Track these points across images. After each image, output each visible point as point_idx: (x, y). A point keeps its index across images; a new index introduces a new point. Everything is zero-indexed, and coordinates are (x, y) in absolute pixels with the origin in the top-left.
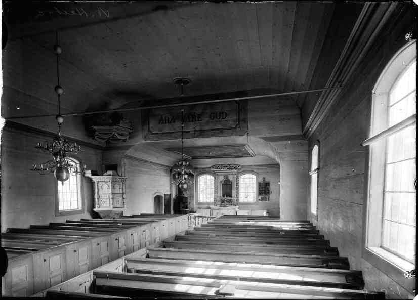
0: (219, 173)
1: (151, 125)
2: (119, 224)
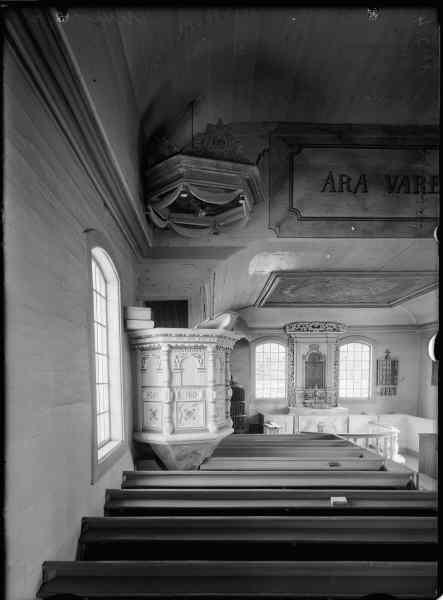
0: (302, 340)
1: (297, 196)
2: (334, 499)
